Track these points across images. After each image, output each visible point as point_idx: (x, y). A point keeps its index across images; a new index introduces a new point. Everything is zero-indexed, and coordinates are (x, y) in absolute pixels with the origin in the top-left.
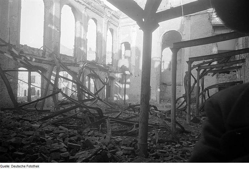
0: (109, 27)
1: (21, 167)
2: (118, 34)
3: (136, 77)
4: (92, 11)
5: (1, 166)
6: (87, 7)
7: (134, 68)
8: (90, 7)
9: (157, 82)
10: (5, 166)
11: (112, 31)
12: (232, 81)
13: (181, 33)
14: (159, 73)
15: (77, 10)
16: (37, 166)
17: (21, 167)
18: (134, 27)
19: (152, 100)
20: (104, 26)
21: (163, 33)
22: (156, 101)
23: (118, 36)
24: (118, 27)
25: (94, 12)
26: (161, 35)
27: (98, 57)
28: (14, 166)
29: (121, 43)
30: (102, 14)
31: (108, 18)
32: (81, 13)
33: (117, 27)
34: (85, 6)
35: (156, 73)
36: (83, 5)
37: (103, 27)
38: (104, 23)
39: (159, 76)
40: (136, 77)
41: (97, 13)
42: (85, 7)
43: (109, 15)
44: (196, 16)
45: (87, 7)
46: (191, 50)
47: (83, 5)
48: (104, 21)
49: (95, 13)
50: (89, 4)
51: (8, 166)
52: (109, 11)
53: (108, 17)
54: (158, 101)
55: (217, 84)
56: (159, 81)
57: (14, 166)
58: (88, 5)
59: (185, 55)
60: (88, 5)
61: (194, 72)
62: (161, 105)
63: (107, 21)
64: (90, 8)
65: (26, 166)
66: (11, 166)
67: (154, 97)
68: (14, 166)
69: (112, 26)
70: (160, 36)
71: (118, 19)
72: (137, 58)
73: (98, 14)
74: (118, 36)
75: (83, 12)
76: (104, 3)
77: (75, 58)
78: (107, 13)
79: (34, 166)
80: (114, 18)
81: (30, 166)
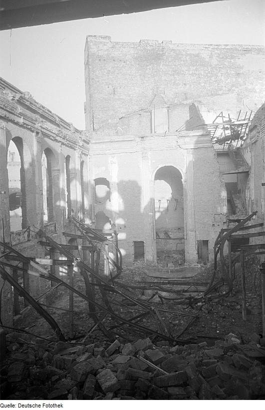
1: (34, 406)
5: (2, 405)
6: (63, 144)
10: (9, 405)
12: (57, 323)
13: (180, 171)
14: (154, 224)
15: (53, 151)
16: (59, 405)
17: (34, 406)
18: (113, 157)
19: (147, 260)
21: (156, 168)
23: (88, 170)
26: (154, 171)
28: (23, 406)
30: (75, 146)
33: (87, 155)
35: (150, 224)
38: (77, 158)
40: (121, 228)
43: (81, 144)
45: (63, 144)
51: (13, 406)
55: (18, 253)
57: (23, 405)
58: (63, 141)
61: (29, 127)
65: (42, 406)
66: (17, 406)
68: (23, 406)
70: (153, 173)
71: (88, 143)
74: (88, 170)
77: (54, 225)
79: (54, 405)
80: (85, 145)
81: (49, 406)
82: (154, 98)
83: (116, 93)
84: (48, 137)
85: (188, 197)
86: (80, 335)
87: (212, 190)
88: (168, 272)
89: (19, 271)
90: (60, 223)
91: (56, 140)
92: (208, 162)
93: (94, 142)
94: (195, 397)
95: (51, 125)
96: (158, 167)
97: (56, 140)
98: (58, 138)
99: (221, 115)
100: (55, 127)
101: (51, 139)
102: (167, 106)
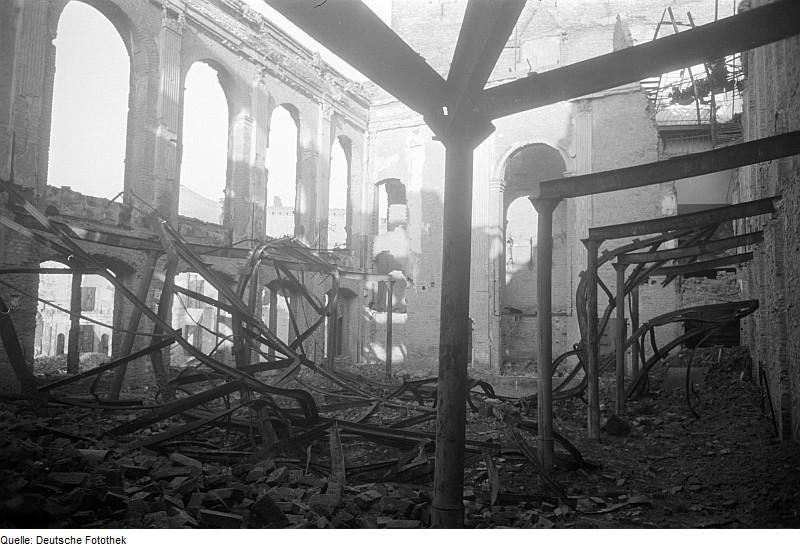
0: (338, 132)
1: (68, 541)
2: (365, 155)
3: (424, 288)
4: (283, 81)
5: (4, 540)
6: (267, 71)
7: (418, 259)
8: (276, 69)
9: (491, 307)
10: (17, 540)
11: (346, 144)
13: (561, 152)
14: (497, 276)
15: (235, 78)
16: (118, 540)
17: (68, 541)
18: (417, 133)
19: (477, 362)
20: (323, 129)
21: (507, 150)
22: (490, 366)
23: (365, 160)
24: (367, 133)
25: (288, 84)
26: (501, 157)
27: (302, 227)
28: (46, 541)
29: (375, 182)
30: (315, 92)
31: (335, 104)
32: (249, 88)
33: (364, 132)
34: (263, 65)
36: (255, 62)
37: (320, 131)
38: (320, 121)
39: (497, 288)
40: (424, 288)
41: (298, 89)
42: (260, 70)
44: (605, 100)
45: (267, 71)
46: (595, 204)
47: (255, 62)
48: (320, 113)
49: (293, 87)
50: (273, 59)
51: (26, 541)
52: (337, 84)
53: (334, 101)
54: (497, 365)
56: (497, 301)
58: (269, 65)
59: (578, 219)
60: (269, 65)
62: (503, 381)
63: (332, 112)
64: (277, 71)
65: (84, 540)
66: (34, 541)
67: (483, 354)
68: (46, 541)
69: (347, 130)
71: (367, 107)
72: (427, 230)
73: (303, 92)
74: (365, 160)
75: (255, 84)
76: (323, 58)
77: (227, 231)
78: (332, 89)
79: (109, 540)
80: (353, 104)
81: (98, 541)
82: (531, 19)
83: (446, 13)
84: (201, 28)
85: (578, 212)
86: (372, 444)
87: (637, 195)
88: (512, 384)
89: (54, 286)
90: (244, 230)
91: (246, 57)
92: (631, 129)
93: (378, 103)
94: (368, 523)
95: (226, 16)
96: (510, 147)
97: (246, 57)
98: (245, 50)
99: (668, 18)
100: (240, 25)
101: (224, 45)
102: (558, 31)
